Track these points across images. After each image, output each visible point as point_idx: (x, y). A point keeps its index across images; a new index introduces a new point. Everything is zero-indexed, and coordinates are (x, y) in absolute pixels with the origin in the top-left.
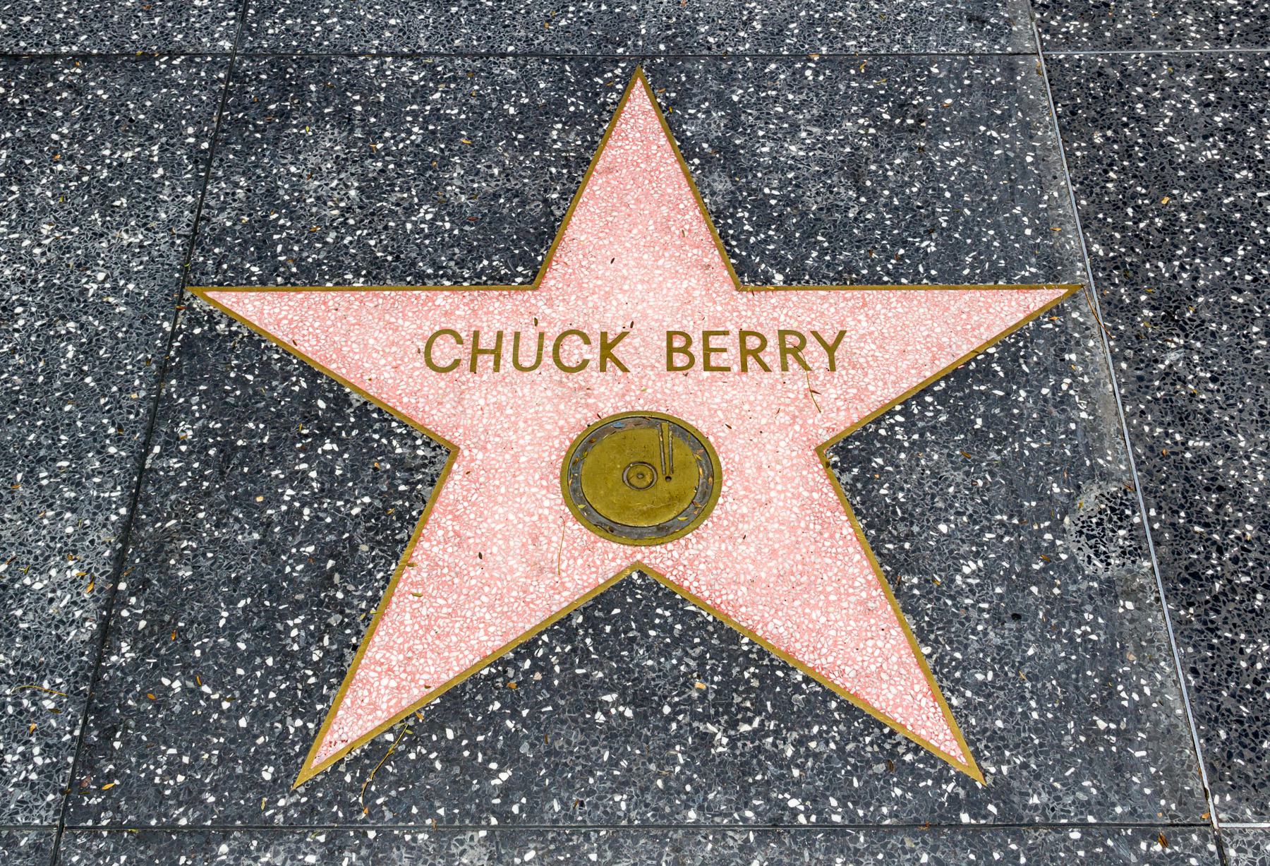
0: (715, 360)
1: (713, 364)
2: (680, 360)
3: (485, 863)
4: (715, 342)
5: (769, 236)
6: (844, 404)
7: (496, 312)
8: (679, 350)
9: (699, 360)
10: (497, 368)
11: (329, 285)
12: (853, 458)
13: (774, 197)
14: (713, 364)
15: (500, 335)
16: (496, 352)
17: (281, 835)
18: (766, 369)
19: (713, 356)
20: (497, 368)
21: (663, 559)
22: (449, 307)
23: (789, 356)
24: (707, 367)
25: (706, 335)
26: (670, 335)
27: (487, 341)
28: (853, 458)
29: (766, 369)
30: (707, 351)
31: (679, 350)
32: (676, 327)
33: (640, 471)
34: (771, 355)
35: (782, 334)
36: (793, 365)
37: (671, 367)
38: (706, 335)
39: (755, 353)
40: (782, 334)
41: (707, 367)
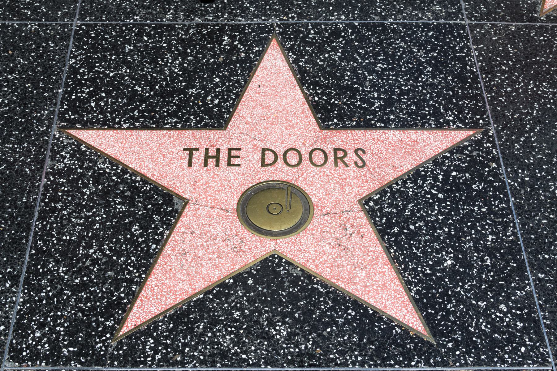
5: (338, 103)
6: (369, 185)
10: (217, 165)
11: (126, 126)
12: (373, 207)
13: (97, 67)
17: (24, 361)
18: (347, 166)
20: (217, 165)
21: (287, 248)
22: (190, 138)
23: (339, 161)
24: (229, 164)
25: (230, 150)
27: (212, 152)
28: (373, 207)
29: (347, 166)
30: (230, 157)
32: (268, 146)
34: (224, 157)
35: (336, 150)
36: (340, 164)
38: (230, 150)
39: (341, 159)
40: (336, 150)
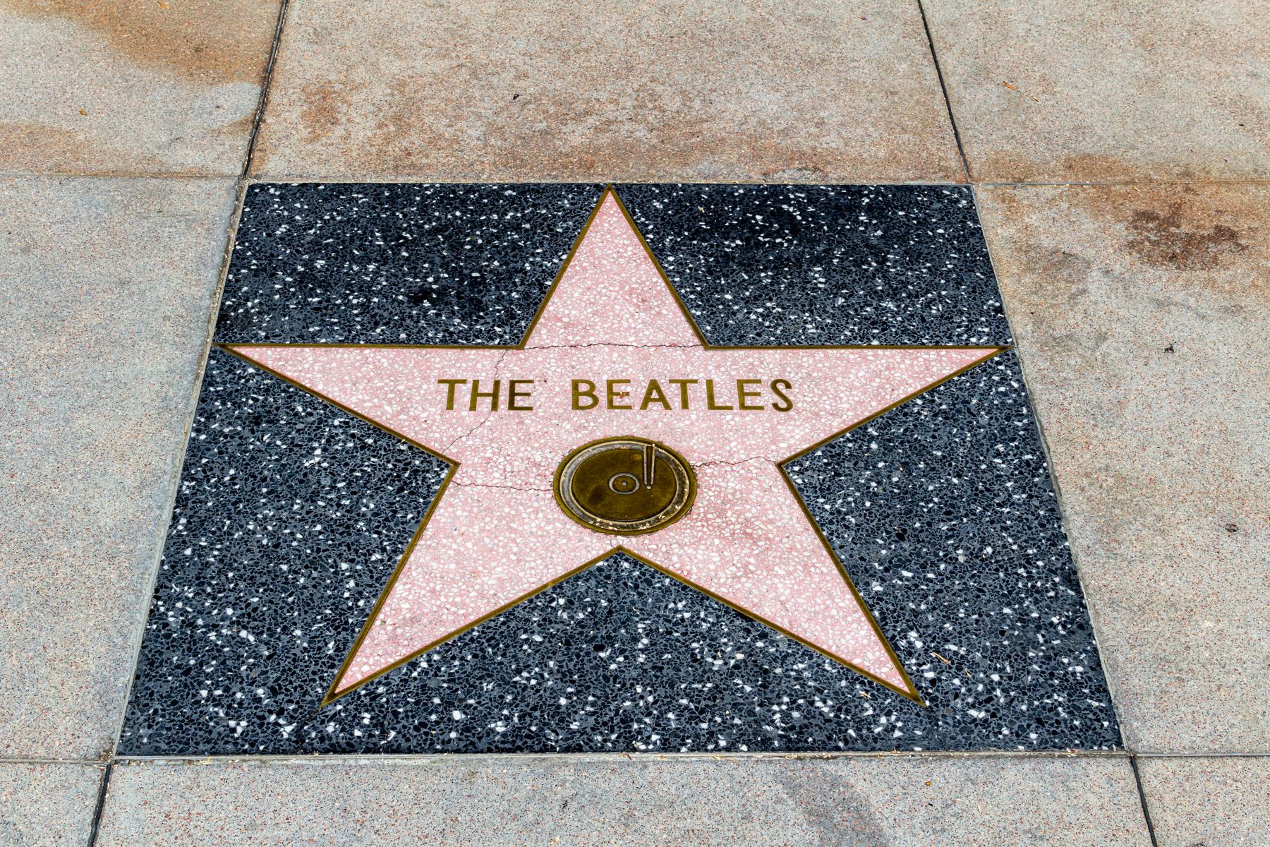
0: (749, 401)
1: (581, 404)
2: (585, 401)
3: (48, 843)
4: (520, 388)
6: (798, 434)
7: (479, 364)
8: (585, 394)
9: (603, 399)
10: (495, 406)
14: (581, 404)
15: (497, 384)
16: (495, 395)
19: (517, 398)
26: (575, 385)
30: (513, 394)
31: (585, 394)
33: (626, 484)
37: (576, 406)
38: (513, 383)
41: (743, 407)
